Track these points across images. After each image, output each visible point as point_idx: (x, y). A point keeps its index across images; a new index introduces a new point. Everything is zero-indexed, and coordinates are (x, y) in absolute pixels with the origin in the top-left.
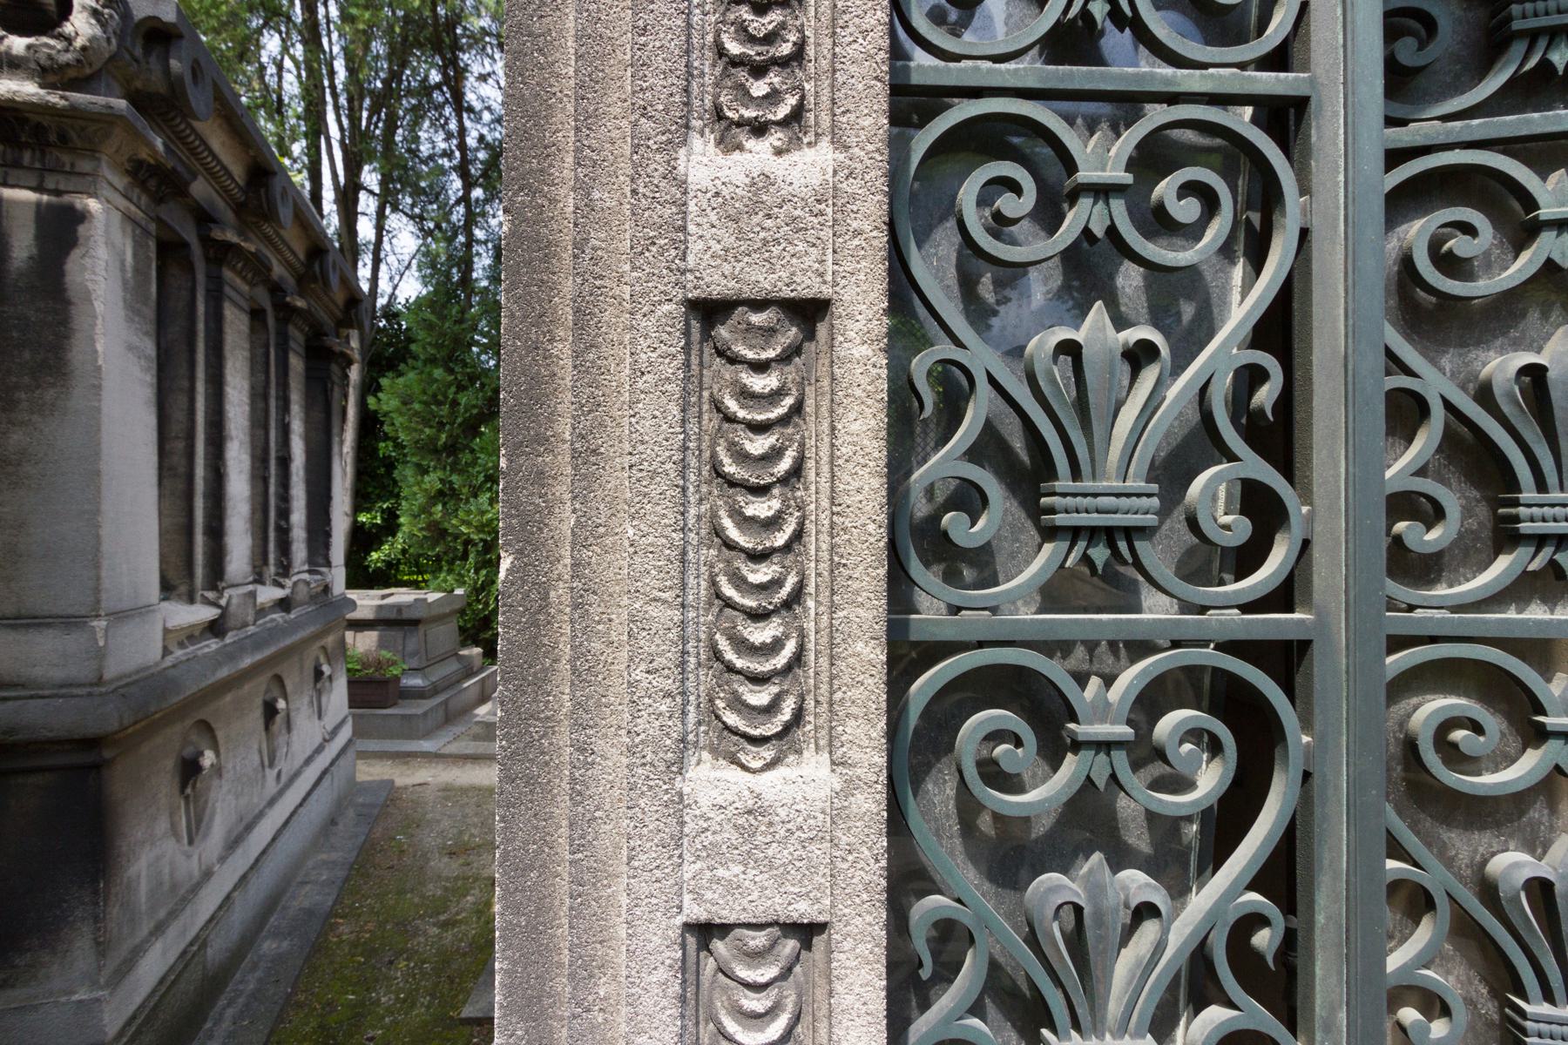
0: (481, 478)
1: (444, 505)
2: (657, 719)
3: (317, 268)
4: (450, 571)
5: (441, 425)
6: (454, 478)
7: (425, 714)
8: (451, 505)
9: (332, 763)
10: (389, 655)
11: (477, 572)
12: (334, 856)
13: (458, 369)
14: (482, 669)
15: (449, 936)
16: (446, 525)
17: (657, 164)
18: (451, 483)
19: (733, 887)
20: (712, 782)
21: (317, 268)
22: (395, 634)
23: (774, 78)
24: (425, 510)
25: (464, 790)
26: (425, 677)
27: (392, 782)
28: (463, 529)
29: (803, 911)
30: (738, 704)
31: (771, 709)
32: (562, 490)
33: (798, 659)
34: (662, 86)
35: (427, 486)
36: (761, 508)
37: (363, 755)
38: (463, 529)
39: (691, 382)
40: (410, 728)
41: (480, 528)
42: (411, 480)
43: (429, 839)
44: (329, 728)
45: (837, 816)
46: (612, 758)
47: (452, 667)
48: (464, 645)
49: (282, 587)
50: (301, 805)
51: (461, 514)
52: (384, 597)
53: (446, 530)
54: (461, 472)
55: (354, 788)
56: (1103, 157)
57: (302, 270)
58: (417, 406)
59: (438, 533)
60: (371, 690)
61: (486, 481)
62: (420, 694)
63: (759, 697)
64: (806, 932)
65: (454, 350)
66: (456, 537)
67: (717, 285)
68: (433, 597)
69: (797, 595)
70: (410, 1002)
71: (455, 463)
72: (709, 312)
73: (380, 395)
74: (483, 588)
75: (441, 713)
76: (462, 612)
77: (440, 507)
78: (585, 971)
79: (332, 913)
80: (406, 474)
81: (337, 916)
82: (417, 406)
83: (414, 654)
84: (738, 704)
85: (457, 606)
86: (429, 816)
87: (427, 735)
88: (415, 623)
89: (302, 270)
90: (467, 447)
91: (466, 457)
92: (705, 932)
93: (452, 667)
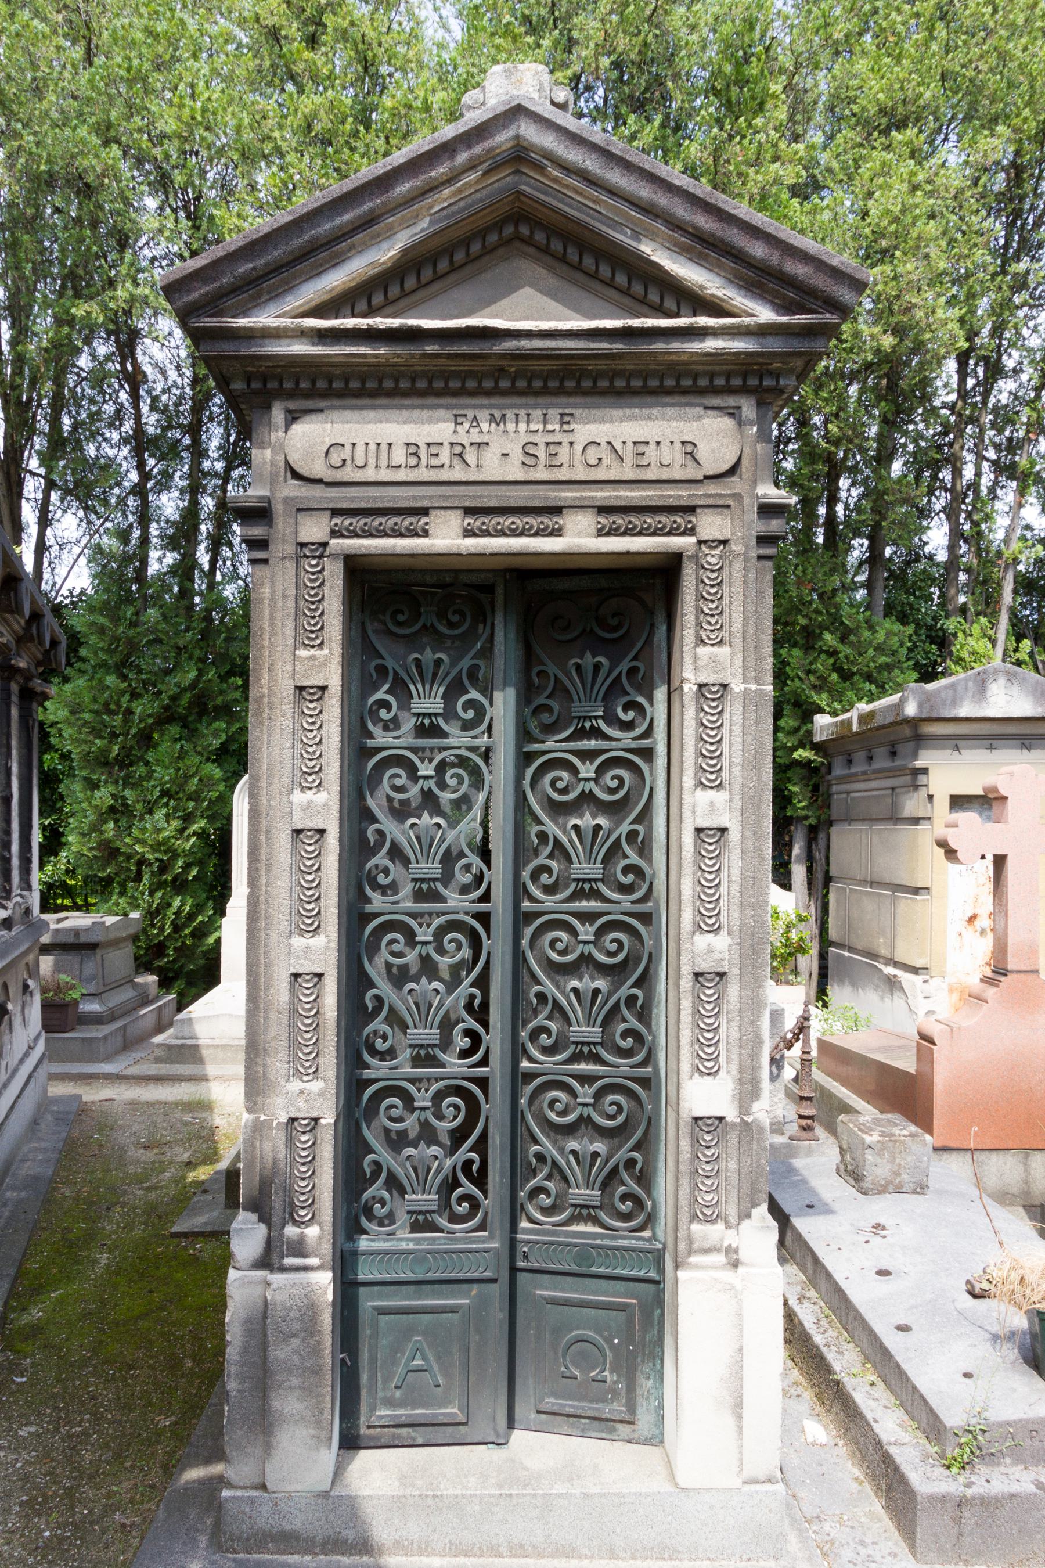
0: (157, 793)
1: (116, 821)
2: (285, 927)
3: (34, 631)
4: (122, 894)
5: (114, 735)
6: (127, 793)
7: (105, 1038)
8: (123, 823)
9: (34, 1070)
10: (68, 979)
11: (151, 894)
12: (43, 1145)
13: (132, 675)
14: (157, 998)
15: (153, 1196)
16: (118, 844)
17: (285, 799)
18: (124, 798)
19: (302, 965)
20: (298, 942)
21: (34, 631)
22: (72, 959)
23: (314, 777)
24: (95, 828)
25: (150, 1104)
26: (102, 1002)
27: (80, 1096)
28: (138, 848)
29: (318, 970)
30: (304, 923)
31: (312, 924)
32: (262, 872)
33: (319, 913)
34: (286, 780)
35: (98, 802)
36: (310, 878)
37: (54, 1077)
38: (138, 848)
39: (294, 847)
40: (90, 1051)
41: (156, 847)
42: (80, 795)
43: (124, 1138)
44: (32, 1037)
45: (327, 948)
46: (274, 936)
47: (126, 995)
48: (138, 973)
49: (6, 908)
50: (18, 1097)
51: (135, 832)
52: (59, 921)
53: (118, 849)
54: (133, 786)
55: (44, 1104)
56: (426, 769)
57: (21, 632)
58: (87, 716)
59: (110, 852)
60: (58, 1015)
61: (162, 796)
62: (97, 1019)
63: (309, 921)
64: (320, 976)
65: (128, 656)
66: (129, 857)
67: (300, 827)
68: (110, 920)
69: (319, 898)
70: (129, 1227)
71: (128, 776)
72: (298, 832)
73: (47, 704)
74: (158, 911)
75: (120, 1039)
76: (135, 938)
77: (111, 825)
78: (268, 987)
79: (52, 1180)
80: (73, 789)
81: (56, 1182)
82: (87, 716)
83: (89, 980)
84: (304, 923)
85: (132, 931)
86: (121, 1122)
87: (108, 1059)
88: (93, 947)
89: (21, 632)
90: (141, 758)
91: (140, 770)
92: (296, 976)
93: (126, 995)
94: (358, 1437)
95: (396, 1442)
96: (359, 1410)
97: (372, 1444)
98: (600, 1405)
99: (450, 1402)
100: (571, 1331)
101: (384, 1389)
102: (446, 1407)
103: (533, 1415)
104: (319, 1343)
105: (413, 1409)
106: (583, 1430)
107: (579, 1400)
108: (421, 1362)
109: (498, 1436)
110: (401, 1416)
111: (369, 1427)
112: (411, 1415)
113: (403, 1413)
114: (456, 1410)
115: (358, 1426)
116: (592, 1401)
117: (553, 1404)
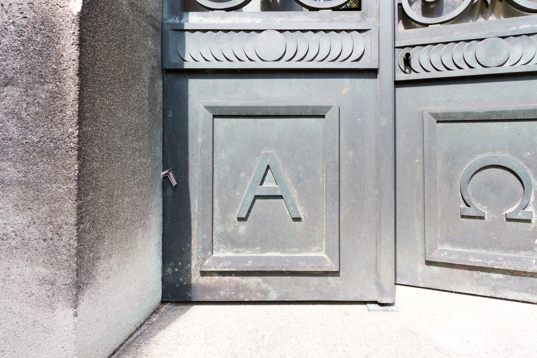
94: (189, 287)
95: (241, 297)
96: (190, 250)
97: (208, 298)
98: (522, 254)
99: (314, 243)
100: (472, 155)
101: (223, 222)
102: (310, 251)
103: (421, 267)
104: (54, 96)
105: (264, 250)
106: (494, 289)
107: (487, 248)
108: (273, 185)
109: (382, 291)
110: (247, 259)
111: (203, 274)
112: (259, 259)
113: (250, 257)
114: (323, 254)
115: (189, 271)
116: (507, 249)
117: (450, 253)
